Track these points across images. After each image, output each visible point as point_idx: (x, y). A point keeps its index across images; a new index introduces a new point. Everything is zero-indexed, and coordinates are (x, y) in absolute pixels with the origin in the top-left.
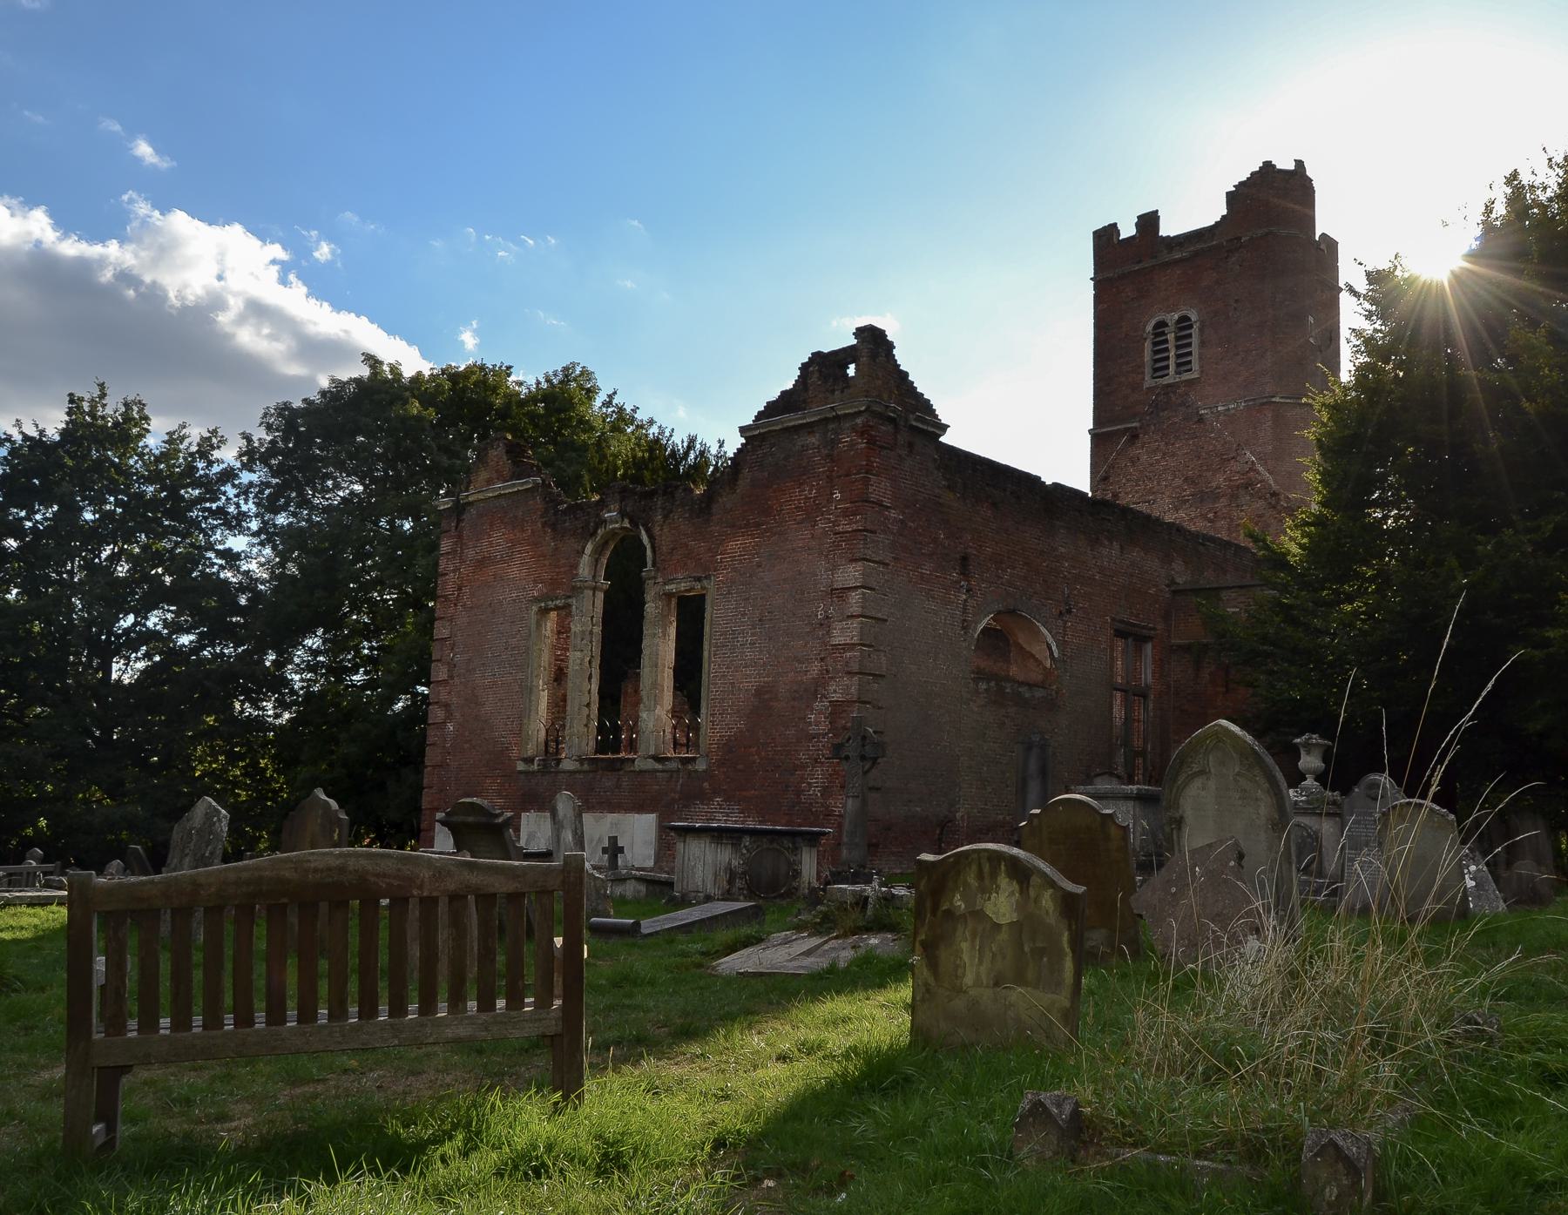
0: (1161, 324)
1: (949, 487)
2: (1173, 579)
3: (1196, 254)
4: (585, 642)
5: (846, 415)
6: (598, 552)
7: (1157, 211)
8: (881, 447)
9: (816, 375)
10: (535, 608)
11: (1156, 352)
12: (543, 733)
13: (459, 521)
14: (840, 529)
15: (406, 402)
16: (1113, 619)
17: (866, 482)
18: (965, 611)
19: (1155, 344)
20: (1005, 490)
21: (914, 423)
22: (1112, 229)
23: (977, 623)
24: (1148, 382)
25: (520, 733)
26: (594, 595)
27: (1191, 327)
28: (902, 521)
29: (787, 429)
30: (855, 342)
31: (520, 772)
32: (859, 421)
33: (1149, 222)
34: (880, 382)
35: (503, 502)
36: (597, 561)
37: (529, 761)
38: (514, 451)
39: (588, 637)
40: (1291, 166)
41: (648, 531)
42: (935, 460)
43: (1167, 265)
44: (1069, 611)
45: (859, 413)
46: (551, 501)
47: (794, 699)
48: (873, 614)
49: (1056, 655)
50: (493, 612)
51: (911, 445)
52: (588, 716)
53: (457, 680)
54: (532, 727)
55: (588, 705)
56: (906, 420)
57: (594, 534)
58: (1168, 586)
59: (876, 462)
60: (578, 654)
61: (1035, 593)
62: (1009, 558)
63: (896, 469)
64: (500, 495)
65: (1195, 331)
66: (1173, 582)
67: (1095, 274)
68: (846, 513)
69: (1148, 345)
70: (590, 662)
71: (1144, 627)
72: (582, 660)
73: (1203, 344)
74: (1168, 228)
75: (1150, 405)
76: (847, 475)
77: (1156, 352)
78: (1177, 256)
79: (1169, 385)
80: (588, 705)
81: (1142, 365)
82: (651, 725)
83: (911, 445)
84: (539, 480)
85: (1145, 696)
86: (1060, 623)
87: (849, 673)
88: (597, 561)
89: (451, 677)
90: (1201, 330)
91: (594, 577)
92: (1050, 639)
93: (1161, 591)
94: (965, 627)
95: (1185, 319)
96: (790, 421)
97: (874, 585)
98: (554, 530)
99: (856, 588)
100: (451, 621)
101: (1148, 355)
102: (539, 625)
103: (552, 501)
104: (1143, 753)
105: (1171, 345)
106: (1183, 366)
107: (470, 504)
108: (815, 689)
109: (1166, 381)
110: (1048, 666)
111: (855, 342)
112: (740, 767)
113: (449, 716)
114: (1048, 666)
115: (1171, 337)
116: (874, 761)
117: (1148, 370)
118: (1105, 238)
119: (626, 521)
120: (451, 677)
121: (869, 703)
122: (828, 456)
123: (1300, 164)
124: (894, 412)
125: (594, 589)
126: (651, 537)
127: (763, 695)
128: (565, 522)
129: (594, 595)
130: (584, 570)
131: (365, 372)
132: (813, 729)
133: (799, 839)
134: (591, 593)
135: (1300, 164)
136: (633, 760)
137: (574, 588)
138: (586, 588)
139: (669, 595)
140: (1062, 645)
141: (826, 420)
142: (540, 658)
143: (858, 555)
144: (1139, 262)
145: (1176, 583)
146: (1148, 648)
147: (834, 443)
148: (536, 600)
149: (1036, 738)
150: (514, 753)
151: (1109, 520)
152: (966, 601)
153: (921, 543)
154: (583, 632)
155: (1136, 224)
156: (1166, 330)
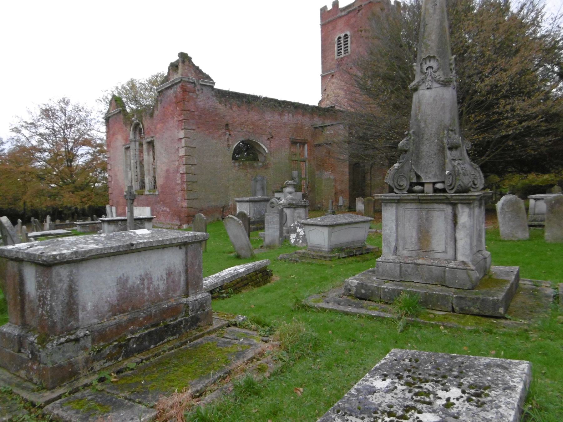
0: (340, 38)
11: (338, 47)
18: (228, 141)
22: (325, 7)
23: (233, 145)
27: (348, 38)
43: (341, 17)
48: (190, 146)
57: (132, 125)
65: (349, 39)
69: (336, 45)
73: (351, 43)
74: (341, 5)
77: (339, 53)
79: (342, 58)
81: (334, 52)
85: (305, 161)
86: (268, 142)
88: (135, 132)
90: (351, 38)
94: (229, 146)
95: (346, 35)
101: (336, 48)
104: (305, 179)
105: (342, 44)
106: (346, 51)
108: (177, 171)
109: (342, 56)
115: (342, 42)
117: (336, 54)
118: (323, 11)
125: (135, 141)
127: (167, 171)
133: (143, 221)
146: (306, 146)
148: (124, 145)
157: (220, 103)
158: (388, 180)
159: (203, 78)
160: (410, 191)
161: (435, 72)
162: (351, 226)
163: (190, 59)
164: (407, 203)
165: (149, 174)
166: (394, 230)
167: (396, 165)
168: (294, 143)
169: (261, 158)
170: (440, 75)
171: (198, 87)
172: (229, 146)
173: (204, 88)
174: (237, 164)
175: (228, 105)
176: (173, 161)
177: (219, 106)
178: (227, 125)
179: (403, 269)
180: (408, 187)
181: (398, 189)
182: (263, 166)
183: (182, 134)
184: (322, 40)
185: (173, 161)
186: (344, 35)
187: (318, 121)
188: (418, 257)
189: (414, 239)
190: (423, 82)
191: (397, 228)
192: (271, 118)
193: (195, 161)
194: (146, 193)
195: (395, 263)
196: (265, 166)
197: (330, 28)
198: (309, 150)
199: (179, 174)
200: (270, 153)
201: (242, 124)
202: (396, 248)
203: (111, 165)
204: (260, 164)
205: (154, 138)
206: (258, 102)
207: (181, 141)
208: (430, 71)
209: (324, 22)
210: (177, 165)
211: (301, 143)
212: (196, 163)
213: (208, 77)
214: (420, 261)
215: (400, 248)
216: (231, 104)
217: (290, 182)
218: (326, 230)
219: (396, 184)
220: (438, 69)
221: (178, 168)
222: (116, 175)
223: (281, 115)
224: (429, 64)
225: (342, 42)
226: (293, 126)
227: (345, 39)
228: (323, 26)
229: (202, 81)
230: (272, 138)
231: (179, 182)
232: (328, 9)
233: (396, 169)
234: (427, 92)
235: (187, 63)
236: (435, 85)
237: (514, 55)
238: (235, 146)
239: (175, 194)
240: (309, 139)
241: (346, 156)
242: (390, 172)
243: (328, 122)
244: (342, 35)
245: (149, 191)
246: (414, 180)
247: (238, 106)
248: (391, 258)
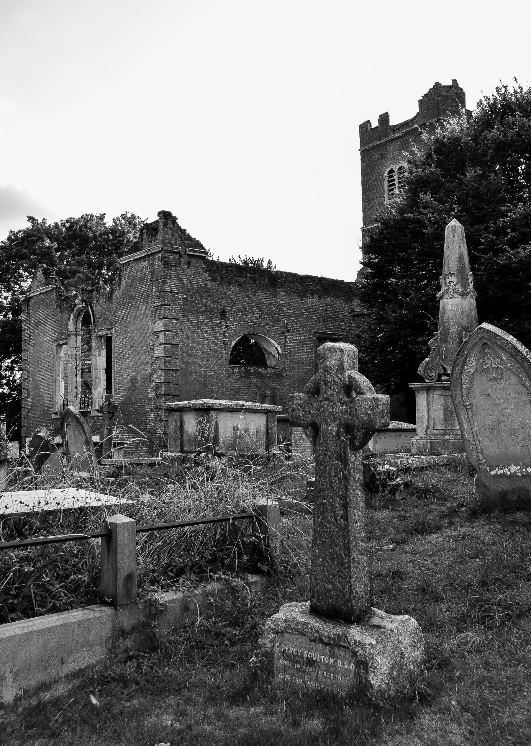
0: (392, 171)
1: (212, 280)
2: (353, 309)
3: (406, 134)
4: (73, 359)
5: (155, 253)
6: (77, 317)
7: (387, 113)
8: (171, 266)
9: (145, 234)
10: (55, 345)
11: (390, 186)
12: (62, 401)
13: (28, 305)
14: (155, 304)
15: (43, 240)
16: (315, 332)
17: (164, 283)
19: (389, 182)
20: (246, 277)
21: (189, 253)
24: (387, 202)
25: (52, 401)
26: (76, 337)
28: (185, 299)
29: (136, 260)
30: (158, 218)
31: (54, 419)
32: (160, 255)
33: (384, 118)
34: (170, 236)
35: (43, 296)
36: (76, 322)
37: (56, 413)
38: (46, 273)
39: (74, 357)
40: (450, 83)
41: (91, 308)
42: (204, 268)
43: (393, 140)
44: (288, 331)
45: (159, 252)
46: (60, 295)
47: (143, 382)
48: (171, 342)
49: (280, 352)
50: (42, 347)
51: (189, 263)
52: (76, 392)
53: (31, 378)
54: (57, 398)
55: (76, 387)
56: (185, 252)
57: (73, 310)
58: (350, 313)
59: (169, 273)
60: (70, 364)
61: (267, 324)
62: (249, 309)
63: (181, 275)
64: (41, 294)
66: (353, 311)
67: (361, 147)
68: (158, 298)
69: (386, 183)
70: (76, 368)
71: (335, 335)
72: (72, 367)
74: (393, 121)
75: (388, 214)
76: (157, 280)
77: (390, 186)
78: (397, 135)
80: (76, 387)
82: (96, 396)
83: (189, 263)
84: (55, 286)
86: (282, 337)
87: (161, 370)
88: (76, 322)
89: (29, 377)
91: (76, 329)
92: (276, 345)
93: (346, 316)
96: (136, 256)
97: (170, 329)
98: (60, 308)
99: (162, 331)
100: (27, 351)
102: (57, 352)
103: (59, 295)
105: (396, 182)
107: (31, 297)
108: (150, 379)
110: (277, 357)
111: (158, 218)
112: (126, 413)
113: (29, 395)
114: (277, 357)
115: (396, 178)
116: (113, 413)
118: (365, 128)
119: (84, 303)
120: (29, 377)
121: (171, 383)
122: (151, 271)
123: (455, 81)
124: (177, 249)
125: (76, 335)
126: (92, 311)
128: (64, 304)
129: (76, 337)
130: (71, 327)
131: (29, 225)
132: (150, 396)
134: (74, 337)
135: (455, 81)
136: (90, 412)
137: (68, 335)
138: (72, 335)
139: (101, 337)
140: (283, 347)
141: (148, 255)
142: (59, 367)
143: (162, 316)
144: (380, 139)
145: (355, 312)
147: (152, 265)
148: (56, 341)
149: (269, 392)
150: (51, 411)
151: (311, 285)
152: (224, 331)
153: (197, 307)
154: (72, 355)
155: (379, 120)
156: (393, 174)
157: (213, 280)
159: (192, 246)
160: (439, 380)
161: (455, 285)
162: (400, 434)
163: (174, 220)
164: (435, 390)
166: (426, 413)
167: (427, 360)
172: (225, 343)
173: (193, 261)
174: (236, 370)
176: (143, 364)
179: (434, 445)
180: (437, 377)
181: (428, 379)
183: (159, 326)
184: (362, 174)
185: (143, 364)
186: (398, 167)
188: (445, 433)
189: (442, 420)
190: (447, 293)
191: (428, 411)
193: (177, 364)
195: (427, 440)
197: (376, 155)
199: (152, 385)
202: (428, 428)
205: (113, 331)
207: (158, 336)
208: (452, 284)
209: (367, 147)
210: (149, 370)
212: (178, 368)
213: (198, 245)
214: (447, 437)
215: (431, 427)
219: (426, 375)
220: (458, 283)
221: (151, 374)
222: (37, 387)
224: (450, 279)
225: (396, 178)
227: (400, 173)
228: (365, 154)
229: (190, 251)
230: (288, 331)
231: (153, 394)
232: (373, 126)
233: (426, 362)
234: (450, 301)
235: (170, 225)
236: (456, 295)
238: (234, 343)
239: (145, 413)
244: (396, 168)
246: (442, 372)
248: (424, 436)
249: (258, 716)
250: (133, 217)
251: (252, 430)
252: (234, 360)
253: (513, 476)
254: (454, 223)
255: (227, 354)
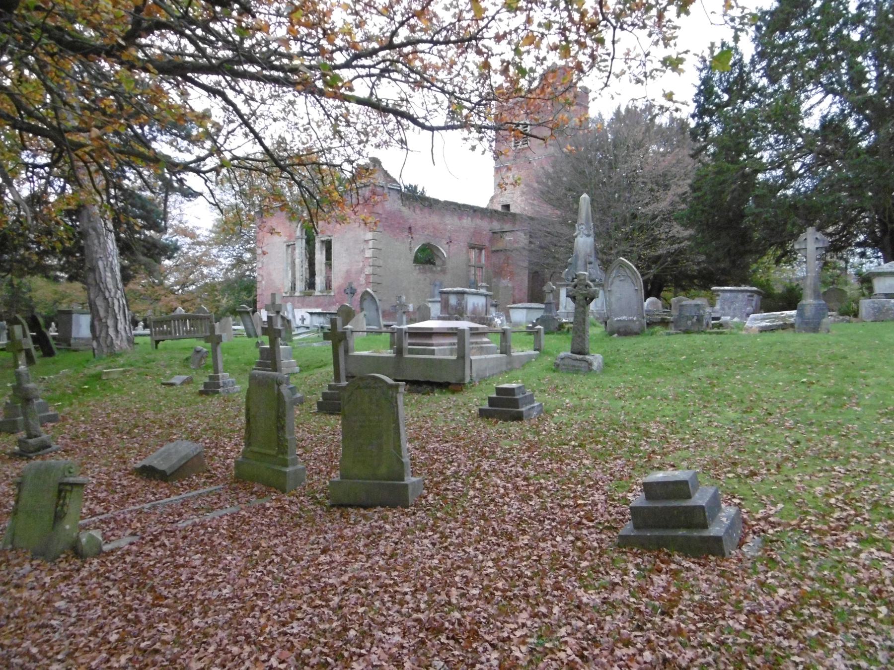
94: (411, 249)
108: (362, 271)
113: (263, 279)
123: (600, 115)
135: (600, 115)
139: (322, 242)
146: (483, 252)
158: (563, 276)
165: (321, 274)
168: (472, 247)
169: (438, 262)
170: (587, 233)
171: (386, 190)
172: (411, 249)
175: (412, 208)
177: (404, 209)
178: (410, 228)
182: (441, 271)
187: (496, 226)
192: (451, 222)
193: (381, 263)
194: (317, 293)
196: (444, 271)
198: (487, 257)
199: (363, 275)
200: (449, 257)
201: (423, 227)
203: (263, 263)
204: (439, 268)
206: (440, 205)
211: (478, 249)
216: (414, 207)
217: (484, 284)
218: (525, 311)
222: (269, 274)
223: (460, 219)
226: (472, 230)
231: (364, 282)
235: (377, 167)
237: (285, 453)
240: (487, 244)
241: (526, 264)
242: (564, 273)
243: (507, 227)
245: (321, 292)
247: (421, 210)
249: (217, 553)
250: (411, 186)
251: (480, 304)
252: (417, 260)
253: (624, 320)
254: (585, 196)
255: (412, 257)
